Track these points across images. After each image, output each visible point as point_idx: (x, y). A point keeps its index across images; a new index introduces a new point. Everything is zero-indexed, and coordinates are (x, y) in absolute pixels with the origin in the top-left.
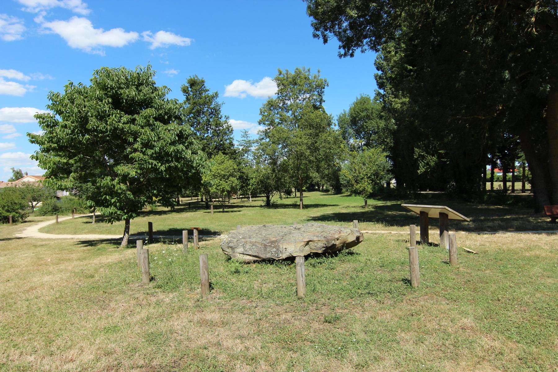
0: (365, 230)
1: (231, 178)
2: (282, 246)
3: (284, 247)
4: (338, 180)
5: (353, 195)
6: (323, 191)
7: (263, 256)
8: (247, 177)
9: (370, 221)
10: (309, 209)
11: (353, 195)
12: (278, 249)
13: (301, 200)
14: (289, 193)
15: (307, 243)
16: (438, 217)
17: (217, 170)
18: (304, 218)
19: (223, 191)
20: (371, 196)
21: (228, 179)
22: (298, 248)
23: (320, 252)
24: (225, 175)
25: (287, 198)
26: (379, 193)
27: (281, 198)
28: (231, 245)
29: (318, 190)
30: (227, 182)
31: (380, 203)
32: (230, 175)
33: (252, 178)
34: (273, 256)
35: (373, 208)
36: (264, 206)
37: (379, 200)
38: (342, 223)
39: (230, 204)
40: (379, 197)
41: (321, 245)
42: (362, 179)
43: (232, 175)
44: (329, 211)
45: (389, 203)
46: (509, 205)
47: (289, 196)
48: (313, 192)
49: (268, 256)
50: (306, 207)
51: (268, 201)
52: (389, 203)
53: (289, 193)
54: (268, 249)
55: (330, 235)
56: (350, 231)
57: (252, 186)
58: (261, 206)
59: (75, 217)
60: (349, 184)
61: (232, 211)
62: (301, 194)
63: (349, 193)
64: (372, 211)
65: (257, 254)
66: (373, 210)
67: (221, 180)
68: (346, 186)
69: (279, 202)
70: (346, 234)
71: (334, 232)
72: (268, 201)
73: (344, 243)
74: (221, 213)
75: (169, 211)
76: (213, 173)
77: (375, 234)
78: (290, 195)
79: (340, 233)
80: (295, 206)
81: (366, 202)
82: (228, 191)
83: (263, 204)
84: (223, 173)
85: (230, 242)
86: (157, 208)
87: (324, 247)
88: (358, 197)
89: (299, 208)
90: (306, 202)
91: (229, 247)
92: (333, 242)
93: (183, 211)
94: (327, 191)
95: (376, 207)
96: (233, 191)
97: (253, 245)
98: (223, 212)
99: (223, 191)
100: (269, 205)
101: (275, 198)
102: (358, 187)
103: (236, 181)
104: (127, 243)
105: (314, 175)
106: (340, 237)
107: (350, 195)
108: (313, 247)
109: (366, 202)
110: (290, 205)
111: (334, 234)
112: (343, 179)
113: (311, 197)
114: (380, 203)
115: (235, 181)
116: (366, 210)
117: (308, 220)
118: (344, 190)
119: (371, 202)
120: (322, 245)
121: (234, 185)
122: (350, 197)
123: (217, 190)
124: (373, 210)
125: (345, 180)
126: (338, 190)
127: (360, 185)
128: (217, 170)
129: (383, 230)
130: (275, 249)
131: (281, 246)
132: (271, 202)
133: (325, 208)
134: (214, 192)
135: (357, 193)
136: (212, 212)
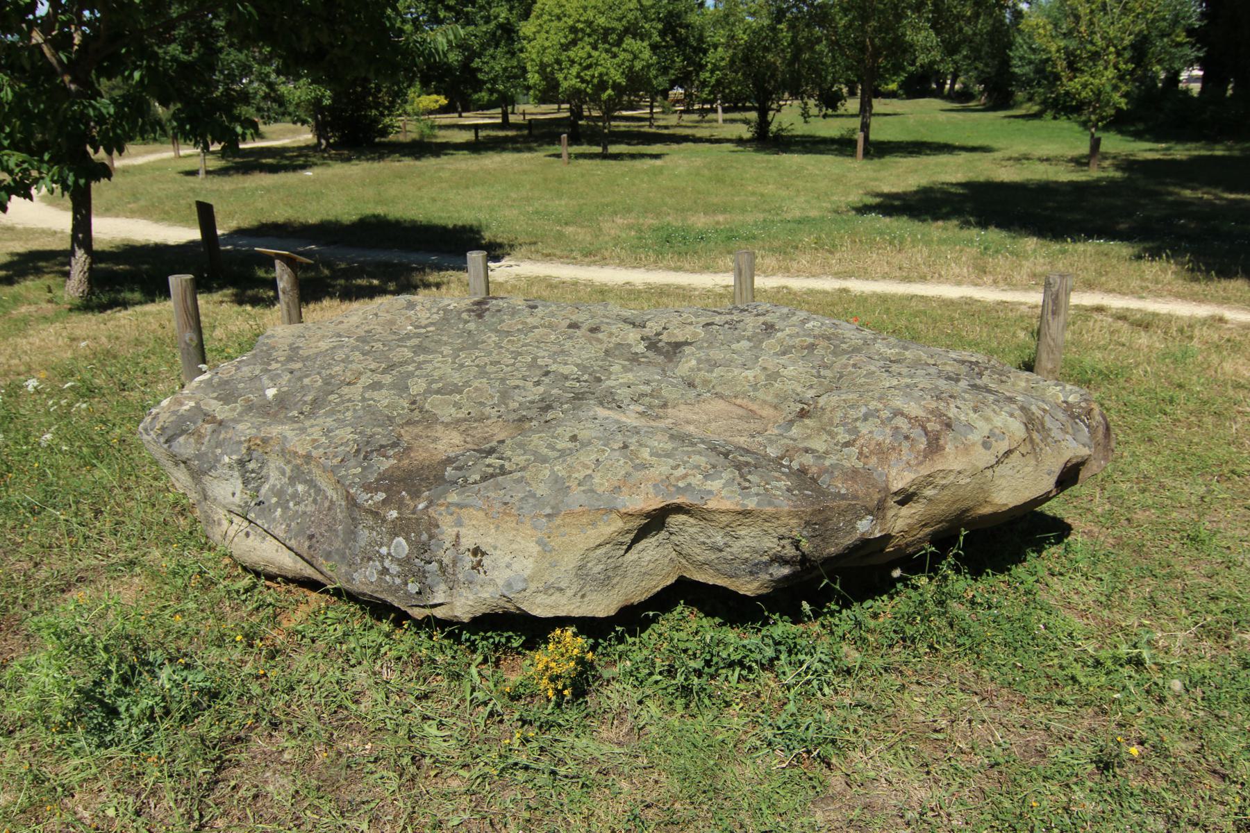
0: (1089, 286)
1: (629, 42)
2: (463, 524)
3: (467, 542)
4: (1006, 62)
5: (1049, 115)
6: (954, 96)
8: (701, 39)
10: (888, 159)
11: (1049, 115)
12: (422, 549)
13: (865, 127)
14: (830, 101)
15: (654, 522)
17: (585, 8)
18: (856, 197)
19: (602, 86)
20: (1120, 123)
21: (619, 43)
22: (570, 561)
23: (748, 587)
24: (607, 31)
25: (825, 116)
26: (1154, 110)
27: (805, 115)
29: (938, 94)
30: (615, 56)
31: (1145, 150)
32: (626, 31)
33: (716, 46)
34: (394, 590)
35: (1118, 167)
36: (748, 141)
37: (1138, 136)
38: (994, 235)
39: (653, 130)
40: (1141, 126)
41: (755, 541)
42: (1095, 56)
43: (632, 30)
44: (950, 171)
45: (1181, 152)
47: (830, 111)
48: (922, 101)
50: (878, 150)
51: (763, 124)
52: (1181, 152)
53: (830, 101)
55: (850, 459)
56: (1017, 428)
57: (712, 72)
58: (740, 141)
59: (182, 153)
60: (1045, 74)
61: (633, 156)
62: (866, 109)
63: (1036, 108)
64: (1112, 181)
66: (1118, 174)
67: (595, 48)
68: (1029, 83)
69: (800, 129)
70: (984, 458)
71: (884, 436)
72: (763, 124)
73: (960, 519)
74: (598, 161)
75: (302, 150)
76: (570, 22)
77: (1145, 323)
78: (835, 108)
79: (934, 446)
80: (843, 146)
81: (1096, 144)
82: (616, 86)
84: (602, 21)
86: (436, 132)
87: (783, 561)
88: (1063, 123)
89: (853, 154)
90: (882, 131)
92: (865, 526)
93: (504, 150)
94: (963, 96)
95: (1129, 165)
96: (636, 84)
98: (605, 156)
99: (602, 86)
100: (767, 140)
101: (788, 116)
102: (1074, 85)
103: (647, 54)
104: (85, 287)
105: (922, 38)
106: (929, 480)
107: (1037, 116)
109: (1096, 144)
110: (832, 141)
111: (882, 452)
112: (1022, 58)
113: (902, 117)
114: (1145, 150)
115: (641, 51)
116: (1092, 174)
117: (863, 210)
118: (1020, 95)
119: (1113, 144)
120: (771, 544)
121: (638, 65)
122: (1036, 123)
123: (583, 81)
124: (1118, 174)
125: (1030, 62)
126: (1000, 94)
127: (1085, 78)
128: (585, 8)
129: (1179, 296)
130: (401, 546)
131: (448, 531)
133: (943, 158)
134: (573, 86)
135: (1066, 107)
136: (565, 157)
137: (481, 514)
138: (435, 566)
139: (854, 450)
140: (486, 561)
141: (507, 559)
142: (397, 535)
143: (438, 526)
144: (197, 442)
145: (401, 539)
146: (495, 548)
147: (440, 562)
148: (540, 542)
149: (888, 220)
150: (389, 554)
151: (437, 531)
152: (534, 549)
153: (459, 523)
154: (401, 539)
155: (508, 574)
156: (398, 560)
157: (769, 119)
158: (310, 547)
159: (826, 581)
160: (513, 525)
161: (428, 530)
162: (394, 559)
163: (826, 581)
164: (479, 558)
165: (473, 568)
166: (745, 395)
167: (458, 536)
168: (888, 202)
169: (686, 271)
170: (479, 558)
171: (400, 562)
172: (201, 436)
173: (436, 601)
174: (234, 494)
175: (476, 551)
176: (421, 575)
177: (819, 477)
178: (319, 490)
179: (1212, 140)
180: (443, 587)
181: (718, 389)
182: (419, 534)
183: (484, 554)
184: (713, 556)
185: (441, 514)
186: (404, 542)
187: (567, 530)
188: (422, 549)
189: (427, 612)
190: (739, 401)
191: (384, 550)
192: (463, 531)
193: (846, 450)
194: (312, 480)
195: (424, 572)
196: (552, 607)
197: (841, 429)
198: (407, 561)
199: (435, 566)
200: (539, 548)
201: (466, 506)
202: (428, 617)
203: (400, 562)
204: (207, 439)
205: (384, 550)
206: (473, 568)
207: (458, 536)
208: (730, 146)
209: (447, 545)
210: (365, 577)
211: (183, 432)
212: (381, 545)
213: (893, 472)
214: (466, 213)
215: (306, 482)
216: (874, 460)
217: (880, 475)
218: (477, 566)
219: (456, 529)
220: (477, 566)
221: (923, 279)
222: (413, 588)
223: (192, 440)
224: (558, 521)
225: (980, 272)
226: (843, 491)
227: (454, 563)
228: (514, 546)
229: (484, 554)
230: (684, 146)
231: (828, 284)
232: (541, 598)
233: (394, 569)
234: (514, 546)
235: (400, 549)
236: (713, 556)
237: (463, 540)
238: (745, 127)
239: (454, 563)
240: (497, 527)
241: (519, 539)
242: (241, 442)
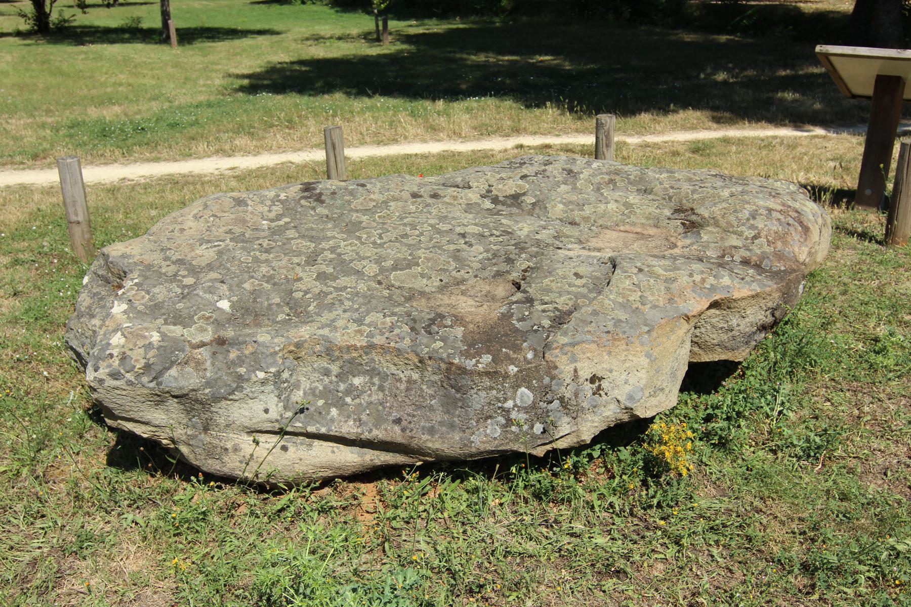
2: (576, 362)
3: (585, 373)
7: (448, 444)
9: (485, 95)
10: (198, 44)
12: (545, 392)
16: (869, 91)
28: (174, 378)
46: (745, 31)
49: (487, 437)
54: (479, 399)
58: (19, 34)
65: (395, 434)
72: (41, 17)
83: (24, 26)
85: (170, 355)
91: (159, 398)
97: (351, 368)
108: (715, 337)
111: (782, 237)
130: (525, 395)
131: (565, 369)
132: (54, 17)
137: (593, 346)
138: (556, 403)
139: (763, 240)
140: (605, 384)
141: (624, 377)
142: (519, 386)
143: (556, 367)
144: (197, 369)
145: (523, 389)
146: (611, 371)
147: (561, 399)
148: (648, 355)
149: (279, 97)
150: (515, 405)
151: (556, 372)
152: (644, 361)
153: (574, 359)
154: (523, 389)
155: (628, 388)
156: (525, 408)
157: (47, 10)
158: (403, 430)
159: (174, 462)
160: (624, 347)
161: (548, 373)
162: (520, 409)
163: (174, 462)
164: (597, 384)
165: (594, 394)
166: (624, 223)
167: (576, 371)
168: (254, 82)
169: (166, 160)
170: (597, 384)
171: (526, 410)
172: (198, 363)
173: (561, 434)
174: (266, 411)
175: (593, 379)
176: (543, 416)
177: (761, 262)
178: (384, 377)
179: (443, 16)
180: (566, 419)
181: (600, 222)
182: (540, 380)
183: (600, 379)
184: (724, 337)
185: (557, 356)
186: (526, 391)
187: (660, 340)
188: (545, 392)
189: (549, 447)
190: (622, 228)
191: (509, 404)
192: (579, 365)
193: (756, 241)
194: (374, 369)
195: (548, 411)
196: (656, 406)
197: (743, 228)
198: (534, 406)
199: (556, 403)
200: (648, 360)
201: (578, 343)
202: (548, 452)
203: (526, 410)
204: (208, 363)
205: (509, 404)
206: (594, 394)
207: (576, 371)
208: (11, 40)
209: (568, 381)
210: (486, 435)
211: (172, 363)
212: (506, 400)
213: (796, 249)
214: (475, 105)
215: (366, 373)
216: (779, 244)
217: (789, 253)
218: (597, 391)
219: (573, 366)
220: (597, 391)
221: (395, 141)
222: (538, 428)
223: (188, 369)
224: (654, 334)
225: (433, 131)
226: (783, 268)
227: (576, 395)
228: (627, 365)
229: (600, 379)
230: (246, 42)
231: (434, 148)
232: (654, 401)
233: (522, 417)
234: (627, 365)
235: (525, 398)
236: (724, 337)
237: (580, 373)
238: (22, 20)
239: (576, 395)
240: (609, 353)
241: (630, 357)
242: (276, 353)
